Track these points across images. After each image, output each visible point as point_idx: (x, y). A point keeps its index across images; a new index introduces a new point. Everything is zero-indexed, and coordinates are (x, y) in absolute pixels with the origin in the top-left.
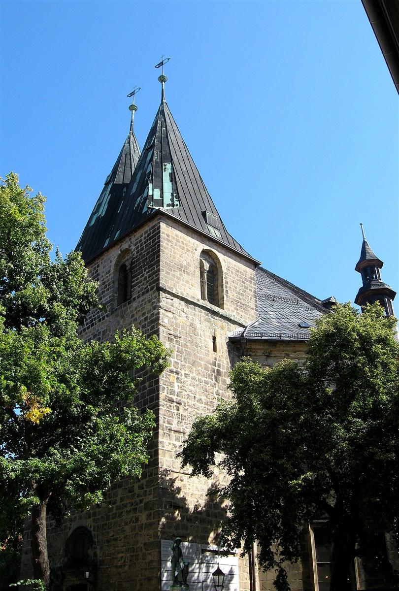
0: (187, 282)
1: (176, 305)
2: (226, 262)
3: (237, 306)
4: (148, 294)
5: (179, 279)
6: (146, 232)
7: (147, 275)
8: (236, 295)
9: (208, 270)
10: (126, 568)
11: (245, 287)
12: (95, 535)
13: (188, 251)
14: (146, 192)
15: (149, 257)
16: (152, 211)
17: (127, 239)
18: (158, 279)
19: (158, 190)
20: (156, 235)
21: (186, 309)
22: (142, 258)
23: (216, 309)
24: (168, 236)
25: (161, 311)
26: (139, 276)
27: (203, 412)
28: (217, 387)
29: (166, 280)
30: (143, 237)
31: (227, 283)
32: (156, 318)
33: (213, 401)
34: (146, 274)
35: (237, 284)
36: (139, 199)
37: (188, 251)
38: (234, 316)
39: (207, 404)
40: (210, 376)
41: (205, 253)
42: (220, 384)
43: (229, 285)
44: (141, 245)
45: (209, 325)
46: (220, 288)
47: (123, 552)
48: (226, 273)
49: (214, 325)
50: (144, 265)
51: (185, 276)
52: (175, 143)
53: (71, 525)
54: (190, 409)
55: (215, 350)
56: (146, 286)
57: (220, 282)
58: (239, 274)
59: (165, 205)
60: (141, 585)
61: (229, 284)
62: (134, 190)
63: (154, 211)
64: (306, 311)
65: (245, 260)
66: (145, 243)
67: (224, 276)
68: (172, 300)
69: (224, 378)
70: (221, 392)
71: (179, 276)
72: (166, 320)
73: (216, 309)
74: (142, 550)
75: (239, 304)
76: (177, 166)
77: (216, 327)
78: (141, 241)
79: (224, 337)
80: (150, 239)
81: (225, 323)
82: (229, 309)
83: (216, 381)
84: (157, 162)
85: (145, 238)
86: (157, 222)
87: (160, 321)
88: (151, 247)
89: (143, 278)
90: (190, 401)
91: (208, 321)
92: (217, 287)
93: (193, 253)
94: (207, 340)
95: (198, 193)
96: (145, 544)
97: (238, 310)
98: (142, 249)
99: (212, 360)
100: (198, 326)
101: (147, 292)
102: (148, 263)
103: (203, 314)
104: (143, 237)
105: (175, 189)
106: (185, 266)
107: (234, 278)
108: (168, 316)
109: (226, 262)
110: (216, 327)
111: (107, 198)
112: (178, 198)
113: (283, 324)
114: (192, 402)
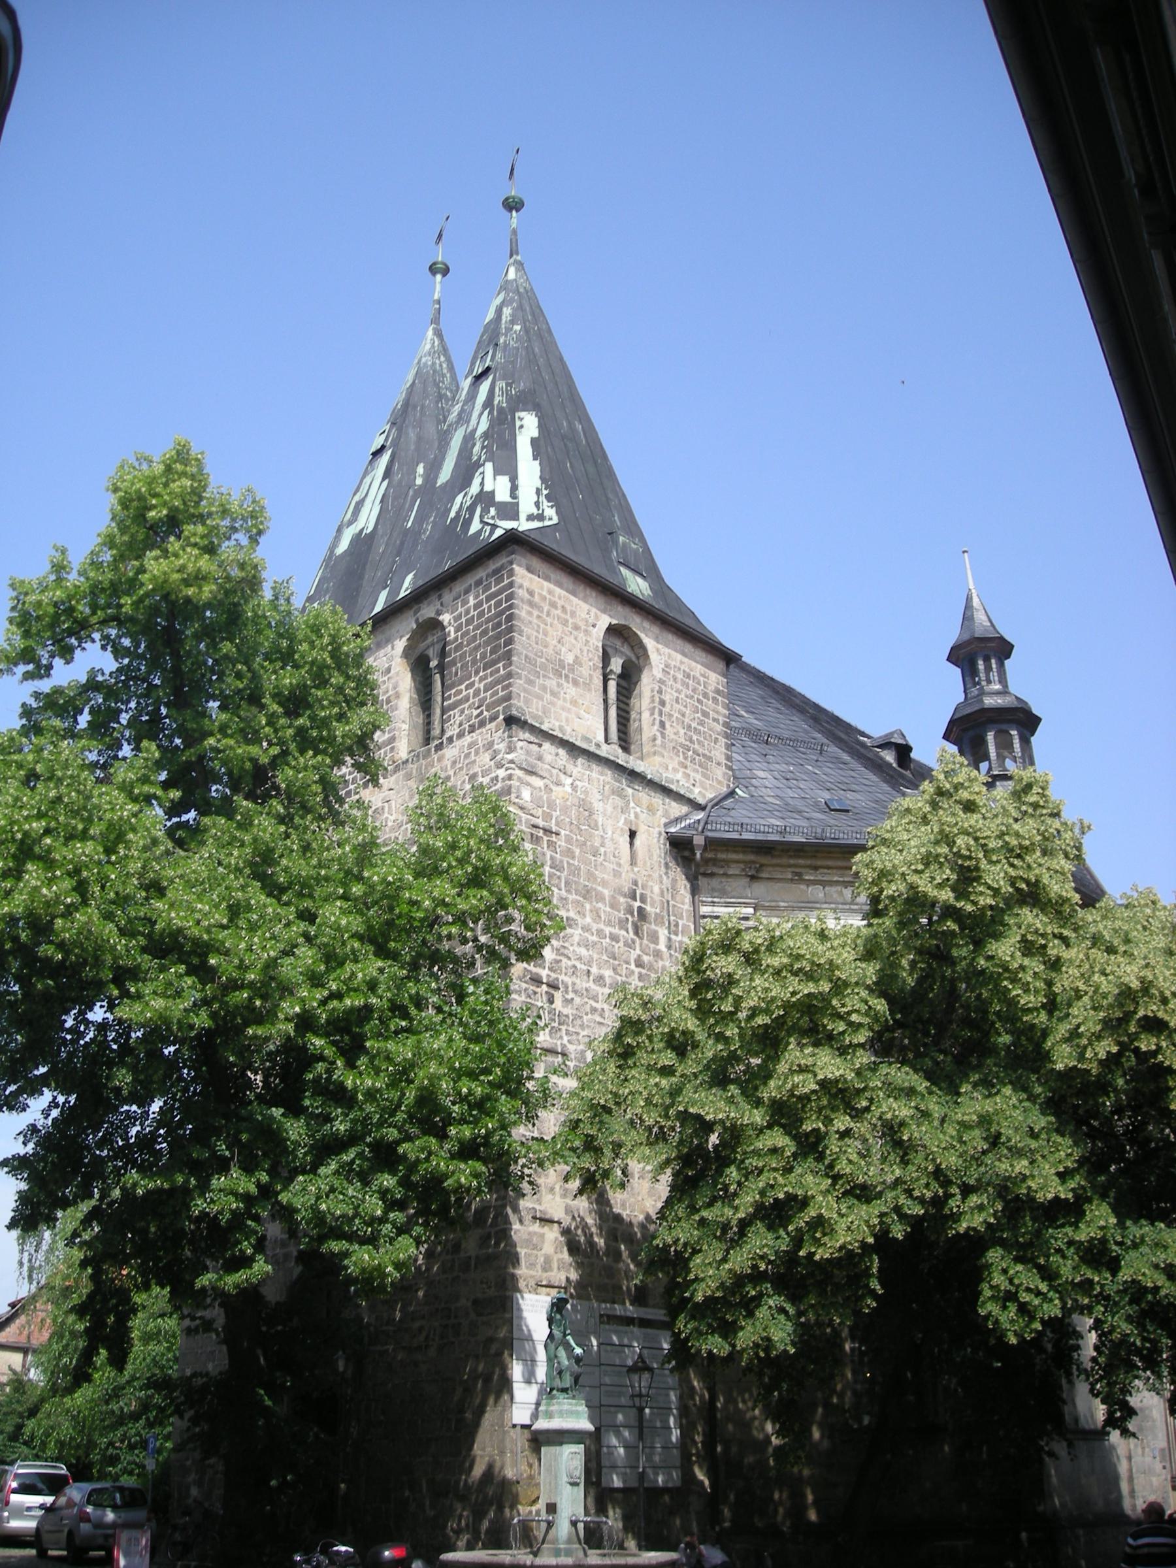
0: (574, 702)
1: (548, 758)
3: (686, 758)
7: (482, 686)
8: (682, 732)
11: (705, 714)
13: (576, 628)
14: (476, 481)
15: (487, 643)
21: (570, 767)
22: (468, 645)
26: (463, 687)
32: (503, 788)
35: (686, 706)
37: (576, 628)
40: (622, 924)
42: (645, 941)
43: (667, 709)
44: (467, 612)
47: (423, 1317)
49: (632, 804)
50: (474, 662)
54: (578, 1000)
61: (668, 706)
63: (499, 533)
65: (704, 650)
66: (476, 606)
69: (653, 927)
70: (646, 958)
71: (556, 689)
72: (526, 794)
77: (638, 810)
81: (657, 800)
83: (636, 933)
88: (488, 620)
89: (471, 691)
91: (620, 793)
97: (686, 767)
100: (598, 806)
101: (482, 724)
102: (483, 656)
108: (528, 784)
114: (582, 984)
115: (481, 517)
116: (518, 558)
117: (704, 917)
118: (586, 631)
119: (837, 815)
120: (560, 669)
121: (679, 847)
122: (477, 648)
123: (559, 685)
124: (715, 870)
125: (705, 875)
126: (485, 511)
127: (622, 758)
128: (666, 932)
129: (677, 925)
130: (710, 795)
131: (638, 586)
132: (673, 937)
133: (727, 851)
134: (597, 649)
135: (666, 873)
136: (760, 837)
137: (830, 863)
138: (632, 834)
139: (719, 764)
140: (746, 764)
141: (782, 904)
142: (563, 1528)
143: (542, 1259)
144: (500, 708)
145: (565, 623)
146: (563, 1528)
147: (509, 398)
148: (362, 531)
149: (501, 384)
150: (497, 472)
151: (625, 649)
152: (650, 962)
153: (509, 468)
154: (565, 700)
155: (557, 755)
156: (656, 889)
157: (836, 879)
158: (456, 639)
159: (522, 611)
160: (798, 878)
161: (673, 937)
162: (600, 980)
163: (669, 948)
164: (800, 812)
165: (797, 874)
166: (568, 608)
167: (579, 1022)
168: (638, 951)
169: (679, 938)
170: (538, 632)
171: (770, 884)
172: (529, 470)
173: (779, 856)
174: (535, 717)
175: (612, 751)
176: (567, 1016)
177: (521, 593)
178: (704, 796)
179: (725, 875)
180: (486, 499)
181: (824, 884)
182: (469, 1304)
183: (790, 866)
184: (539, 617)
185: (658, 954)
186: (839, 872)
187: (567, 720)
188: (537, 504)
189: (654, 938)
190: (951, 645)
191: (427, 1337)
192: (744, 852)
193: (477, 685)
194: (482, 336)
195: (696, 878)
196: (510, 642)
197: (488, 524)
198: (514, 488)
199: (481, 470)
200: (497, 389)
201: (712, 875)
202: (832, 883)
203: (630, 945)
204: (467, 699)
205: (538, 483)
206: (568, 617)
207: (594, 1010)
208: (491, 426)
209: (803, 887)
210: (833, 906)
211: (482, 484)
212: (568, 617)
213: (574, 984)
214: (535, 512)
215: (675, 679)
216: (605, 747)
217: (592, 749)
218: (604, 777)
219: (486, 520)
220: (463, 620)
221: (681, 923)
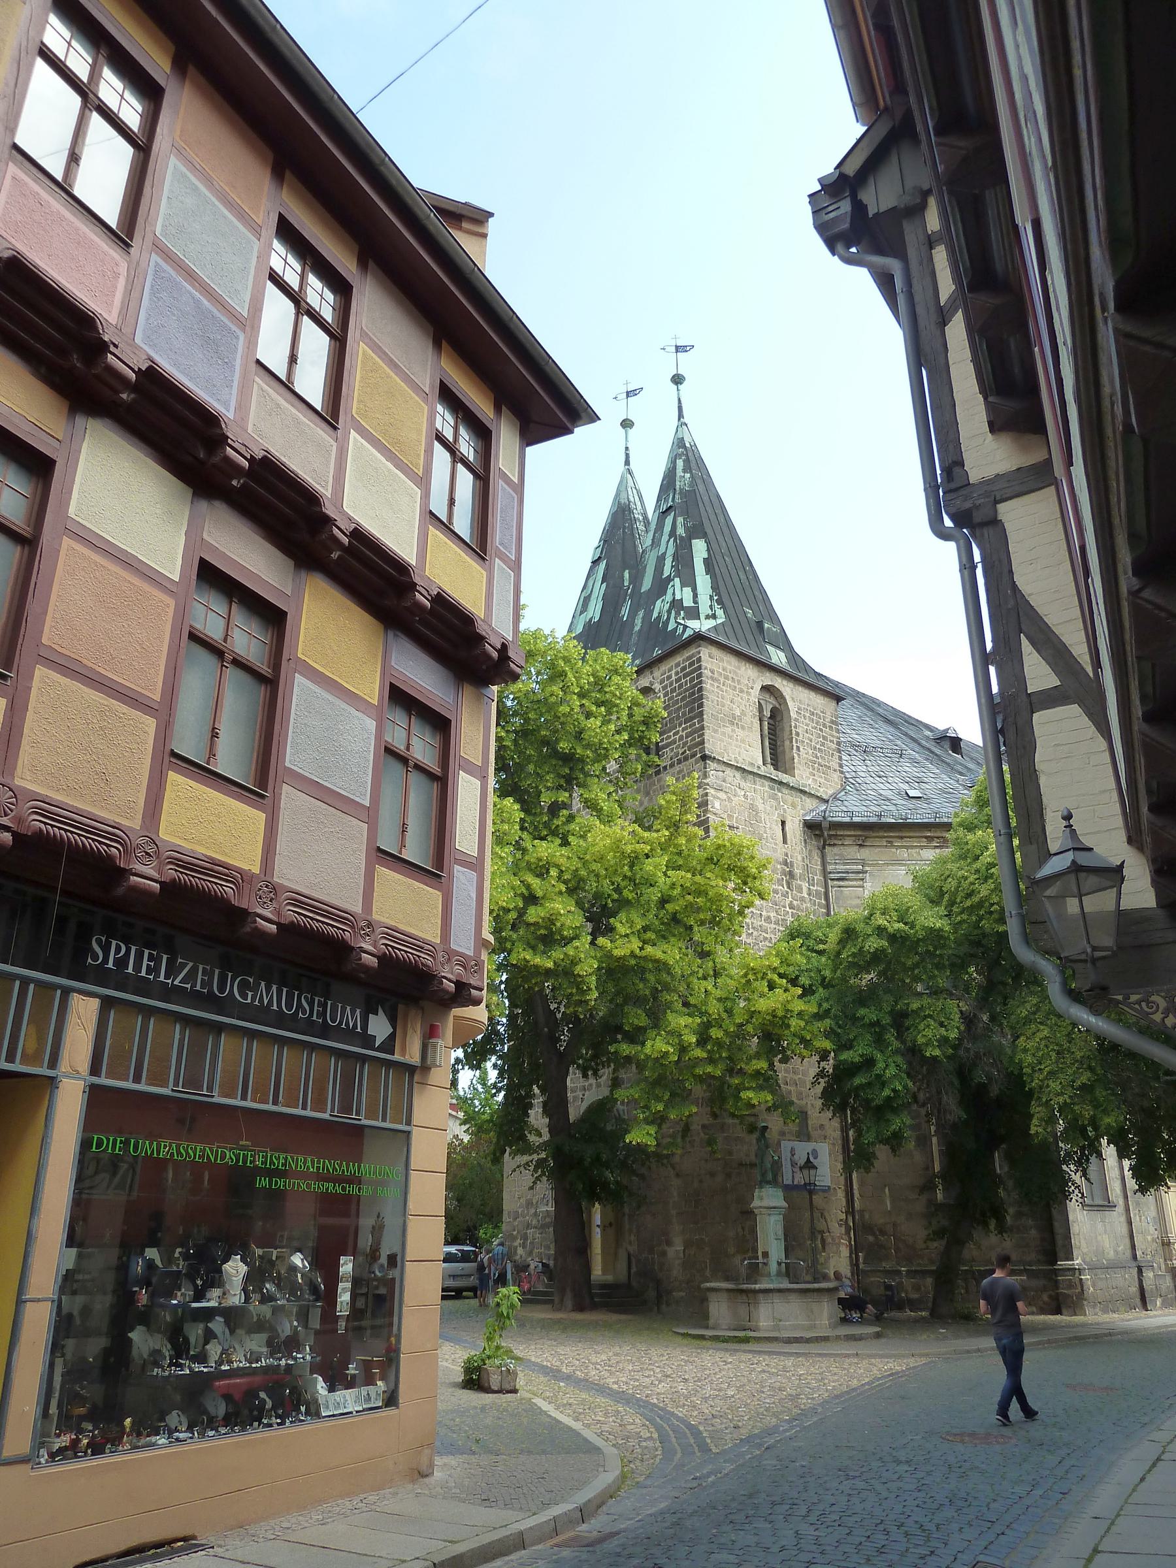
0: (743, 741)
1: (729, 779)
2: (795, 697)
3: (814, 769)
4: (687, 763)
5: (731, 737)
6: (678, 665)
7: (684, 734)
8: (811, 752)
9: (769, 716)
11: (825, 738)
12: (623, 1110)
13: (742, 691)
14: (670, 591)
15: (686, 706)
16: (684, 631)
17: (647, 673)
18: (702, 742)
19: (689, 589)
20: (695, 670)
21: (743, 784)
22: (673, 706)
23: (785, 778)
24: (712, 672)
25: (711, 791)
26: (671, 734)
27: (773, 936)
28: (790, 897)
29: (715, 743)
30: (673, 672)
31: (798, 734)
32: (702, 801)
33: (786, 918)
34: (683, 731)
35: (812, 735)
36: (659, 602)
37: (742, 691)
38: (809, 785)
39: (777, 923)
40: (780, 882)
41: (766, 689)
42: (794, 892)
43: (800, 738)
44: (671, 684)
45: (774, 803)
46: (787, 743)
48: (796, 720)
49: (782, 804)
50: (678, 717)
51: (739, 732)
52: (706, 498)
53: (584, 1095)
54: (755, 933)
55: (785, 841)
56: (683, 750)
57: (786, 734)
58: (815, 718)
59: (702, 616)
60: (701, 1181)
61: (801, 736)
62: (673, 612)
63: (689, 633)
64: (916, 767)
65: (822, 694)
67: (793, 724)
68: (724, 772)
69: (799, 882)
70: (795, 903)
71: (731, 734)
72: (717, 804)
73: (785, 778)
74: (699, 1133)
75: (816, 765)
76: (715, 546)
77: (786, 807)
78: (669, 677)
79: (797, 821)
80: (685, 676)
81: (798, 799)
82: (803, 776)
83: (789, 888)
84: (681, 537)
85: (677, 673)
86: (694, 651)
87: (709, 806)
88: (686, 690)
89: (677, 737)
90: (755, 921)
91: (774, 797)
92: (783, 742)
93: (748, 693)
94: (774, 826)
95: (749, 592)
96: (704, 1126)
97: (814, 775)
98: (673, 691)
99: (781, 858)
100: (761, 807)
101: (686, 759)
103: (767, 789)
104: (673, 672)
105: (715, 587)
106: (738, 716)
107: (807, 725)
108: (718, 798)
109: (795, 697)
110: (786, 807)
111: (599, 589)
112: (719, 602)
113: (881, 792)
114: (757, 923)
115: (676, 618)
116: (703, 649)
117: (830, 873)
118: (747, 692)
119: (914, 801)
120: (733, 721)
121: (813, 828)
123: (733, 731)
124: (836, 842)
125: (829, 845)
126: (678, 614)
127: (774, 774)
128: (807, 885)
129: (813, 880)
130: (830, 792)
131: (778, 657)
132: (811, 887)
133: (844, 830)
134: (755, 703)
135: (805, 847)
136: (865, 819)
137: (911, 834)
138: (783, 823)
139: (835, 770)
140: (852, 767)
141: (881, 862)
142: (773, 1267)
144: (698, 749)
146: (773, 1267)
147: (687, 529)
148: (591, 620)
149: (680, 520)
150: (683, 585)
151: (772, 700)
152: (798, 905)
153: (690, 581)
154: (737, 740)
155: (734, 776)
156: (800, 858)
157: (915, 844)
160: (891, 844)
161: (811, 887)
162: (768, 919)
163: (809, 894)
164: (889, 800)
165: (889, 842)
166: (736, 678)
167: (757, 947)
168: (790, 899)
169: (815, 888)
170: (718, 697)
171: (872, 849)
172: (703, 581)
173: (878, 832)
174: (719, 754)
175: (769, 770)
176: (750, 944)
177: (706, 672)
178: (826, 793)
180: (676, 605)
181: (907, 847)
183: (885, 837)
184: (718, 687)
185: (802, 899)
186: (918, 840)
187: (739, 753)
188: (711, 607)
189: (800, 889)
190: (938, 539)
192: (854, 830)
193: (681, 733)
194: (663, 481)
195: (824, 848)
196: (701, 705)
197: (681, 624)
198: (695, 596)
199: (671, 584)
200: (678, 523)
201: (834, 845)
202: (913, 847)
203: (785, 895)
204: (674, 742)
206: (736, 685)
207: (765, 939)
208: (676, 551)
209: (894, 850)
210: (914, 862)
212: (736, 685)
213: (752, 923)
214: (710, 612)
215: (805, 716)
216: (763, 768)
217: (755, 771)
218: (764, 788)
219: (678, 621)
220: (669, 689)
221: (815, 878)
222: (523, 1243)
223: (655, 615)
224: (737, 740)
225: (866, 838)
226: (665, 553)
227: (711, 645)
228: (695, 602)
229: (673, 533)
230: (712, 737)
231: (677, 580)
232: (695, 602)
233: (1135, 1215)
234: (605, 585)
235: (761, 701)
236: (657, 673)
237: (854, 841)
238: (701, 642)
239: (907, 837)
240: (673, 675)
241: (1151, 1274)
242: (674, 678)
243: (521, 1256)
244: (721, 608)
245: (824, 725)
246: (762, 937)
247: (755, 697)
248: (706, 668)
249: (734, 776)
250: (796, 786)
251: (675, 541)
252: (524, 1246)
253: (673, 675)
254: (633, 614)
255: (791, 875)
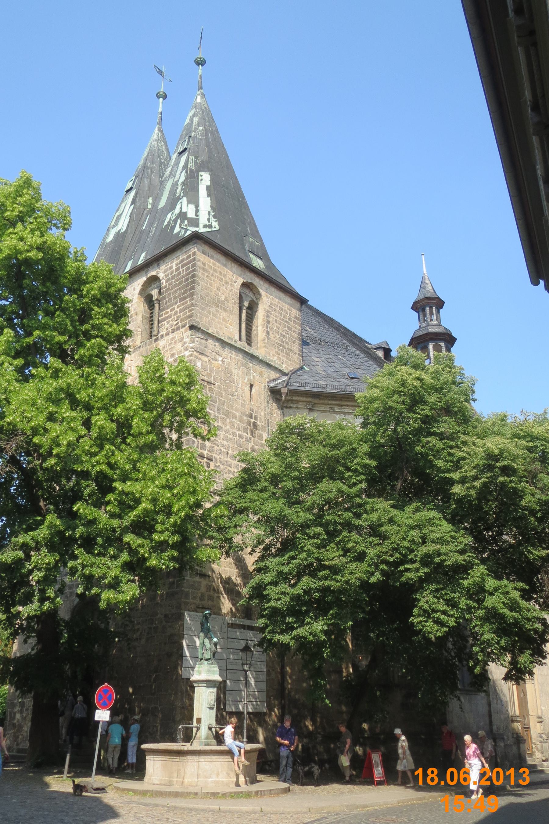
1: (211, 347)
3: (279, 350)
4: (179, 332)
5: (214, 315)
10: (143, 641)
13: (227, 283)
14: (178, 207)
16: (185, 233)
21: (221, 352)
22: (172, 289)
26: (169, 310)
28: (252, 442)
35: (280, 324)
36: (169, 215)
37: (227, 283)
40: (245, 430)
42: (256, 439)
44: (172, 273)
45: (245, 370)
49: (252, 371)
56: (176, 322)
61: (271, 324)
69: (260, 432)
70: (256, 447)
71: (215, 313)
77: (255, 374)
80: (183, 266)
83: (252, 435)
84: (191, 171)
88: (183, 277)
89: (173, 312)
90: (222, 457)
91: (247, 367)
96: (166, 616)
97: (279, 354)
98: (173, 277)
99: (248, 412)
100: (235, 371)
101: (178, 329)
102: (180, 295)
106: (222, 301)
107: (277, 317)
108: (200, 359)
115: (180, 225)
120: (218, 303)
121: (275, 393)
122: (176, 291)
123: (217, 311)
124: (292, 405)
126: (182, 222)
128: (267, 435)
131: (258, 263)
136: (314, 389)
138: (251, 386)
143: (200, 595)
145: (221, 280)
150: (189, 202)
153: (194, 200)
154: (220, 318)
155: (215, 345)
158: (166, 286)
159: (199, 273)
165: (332, 408)
166: (223, 272)
168: (252, 444)
170: (207, 283)
172: (205, 202)
174: (204, 326)
175: (243, 345)
178: (288, 369)
179: (297, 407)
180: (183, 216)
181: (345, 414)
182: (163, 616)
183: (329, 404)
184: (208, 276)
187: (221, 329)
188: (209, 220)
189: (261, 437)
191: (141, 633)
193: (176, 309)
197: (184, 228)
198: (197, 211)
199: (180, 201)
203: (249, 440)
204: (171, 316)
205: (209, 209)
206: (222, 277)
207: (230, 472)
209: (335, 415)
211: (181, 208)
212: (222, 277)
213: (220, 458)
214: (207, 223)
215: (275, 310)
216: (239, 342)
217: (233, 343)
220: (170, 276)
222: (21, 710)
223: (166, 223)
224: (220, 318)
225: (315, 404)
226: (178, 181)
227: (205, 244)
228: (197, 215)
229: (185, 167)
230: (200, 313)
231: (185, 200)
232: (197, 215)
233: (493, 699)
234: (133, 206)
235: (242, 294)
236: (163, 267)
237: (306, 406)
238: (197, 240)
239: (345, 406)
240: (174, 266)
241: (502, 744)
242: (174, 268)
243: (18, 721)
244: (216, 221)
245: (290, 319)
246: (227, 470)
247: (237, 289)
248: (199, 261)
249: (215, 345)
250: (264, 360)
251: (186, 172)
252: (21, 712)
253: (174, 266)
254: (150, 225)
255: (255, 426)
